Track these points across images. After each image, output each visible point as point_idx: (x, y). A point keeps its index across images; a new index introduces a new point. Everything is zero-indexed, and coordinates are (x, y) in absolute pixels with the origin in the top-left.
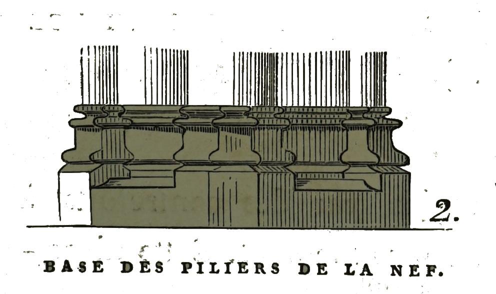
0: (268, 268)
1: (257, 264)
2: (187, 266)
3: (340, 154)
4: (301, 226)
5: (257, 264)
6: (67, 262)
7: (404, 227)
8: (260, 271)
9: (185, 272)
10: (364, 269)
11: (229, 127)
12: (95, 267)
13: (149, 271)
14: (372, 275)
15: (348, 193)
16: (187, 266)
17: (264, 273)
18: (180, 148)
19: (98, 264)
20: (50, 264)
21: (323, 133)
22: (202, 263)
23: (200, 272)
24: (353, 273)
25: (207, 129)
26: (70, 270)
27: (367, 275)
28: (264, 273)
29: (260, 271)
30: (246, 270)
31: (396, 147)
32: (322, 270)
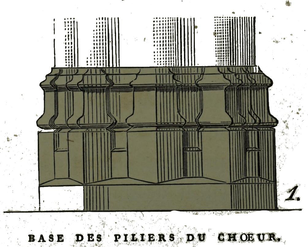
0: (167, 238)
1: (160, 235)
2: (118, 237)
3: (67, 120)
4: (88, 209)
5: (160, 235)
6: (42, 236)
7: (235, 209)
8: (272, 238)
9: (116, 240)
10: (40, 237)
11: (162, 88)
12: (150, 238)
13: (154, 240)
14: (45, 241)
15: (192, 176)
16: (118, 237)
17: (165, 241)
18: (128, 119)
19: (151, 236)
20: (162, 236)
21: (184, 92)
22: (127, 235)
23: (126, 240)
24: (136, 240)
25: (93, 90)
26: (44, 241)
27: (42, 242)
28: (165, 241)
29: (272, 238)
30: (92, 239)
31: (272, 113)
32: (250, 238)
